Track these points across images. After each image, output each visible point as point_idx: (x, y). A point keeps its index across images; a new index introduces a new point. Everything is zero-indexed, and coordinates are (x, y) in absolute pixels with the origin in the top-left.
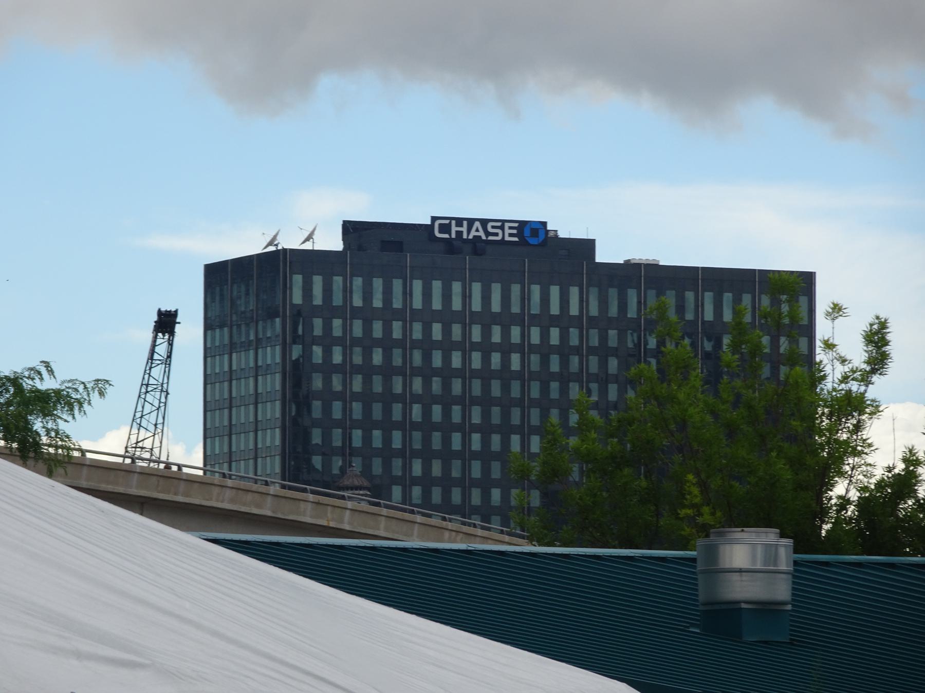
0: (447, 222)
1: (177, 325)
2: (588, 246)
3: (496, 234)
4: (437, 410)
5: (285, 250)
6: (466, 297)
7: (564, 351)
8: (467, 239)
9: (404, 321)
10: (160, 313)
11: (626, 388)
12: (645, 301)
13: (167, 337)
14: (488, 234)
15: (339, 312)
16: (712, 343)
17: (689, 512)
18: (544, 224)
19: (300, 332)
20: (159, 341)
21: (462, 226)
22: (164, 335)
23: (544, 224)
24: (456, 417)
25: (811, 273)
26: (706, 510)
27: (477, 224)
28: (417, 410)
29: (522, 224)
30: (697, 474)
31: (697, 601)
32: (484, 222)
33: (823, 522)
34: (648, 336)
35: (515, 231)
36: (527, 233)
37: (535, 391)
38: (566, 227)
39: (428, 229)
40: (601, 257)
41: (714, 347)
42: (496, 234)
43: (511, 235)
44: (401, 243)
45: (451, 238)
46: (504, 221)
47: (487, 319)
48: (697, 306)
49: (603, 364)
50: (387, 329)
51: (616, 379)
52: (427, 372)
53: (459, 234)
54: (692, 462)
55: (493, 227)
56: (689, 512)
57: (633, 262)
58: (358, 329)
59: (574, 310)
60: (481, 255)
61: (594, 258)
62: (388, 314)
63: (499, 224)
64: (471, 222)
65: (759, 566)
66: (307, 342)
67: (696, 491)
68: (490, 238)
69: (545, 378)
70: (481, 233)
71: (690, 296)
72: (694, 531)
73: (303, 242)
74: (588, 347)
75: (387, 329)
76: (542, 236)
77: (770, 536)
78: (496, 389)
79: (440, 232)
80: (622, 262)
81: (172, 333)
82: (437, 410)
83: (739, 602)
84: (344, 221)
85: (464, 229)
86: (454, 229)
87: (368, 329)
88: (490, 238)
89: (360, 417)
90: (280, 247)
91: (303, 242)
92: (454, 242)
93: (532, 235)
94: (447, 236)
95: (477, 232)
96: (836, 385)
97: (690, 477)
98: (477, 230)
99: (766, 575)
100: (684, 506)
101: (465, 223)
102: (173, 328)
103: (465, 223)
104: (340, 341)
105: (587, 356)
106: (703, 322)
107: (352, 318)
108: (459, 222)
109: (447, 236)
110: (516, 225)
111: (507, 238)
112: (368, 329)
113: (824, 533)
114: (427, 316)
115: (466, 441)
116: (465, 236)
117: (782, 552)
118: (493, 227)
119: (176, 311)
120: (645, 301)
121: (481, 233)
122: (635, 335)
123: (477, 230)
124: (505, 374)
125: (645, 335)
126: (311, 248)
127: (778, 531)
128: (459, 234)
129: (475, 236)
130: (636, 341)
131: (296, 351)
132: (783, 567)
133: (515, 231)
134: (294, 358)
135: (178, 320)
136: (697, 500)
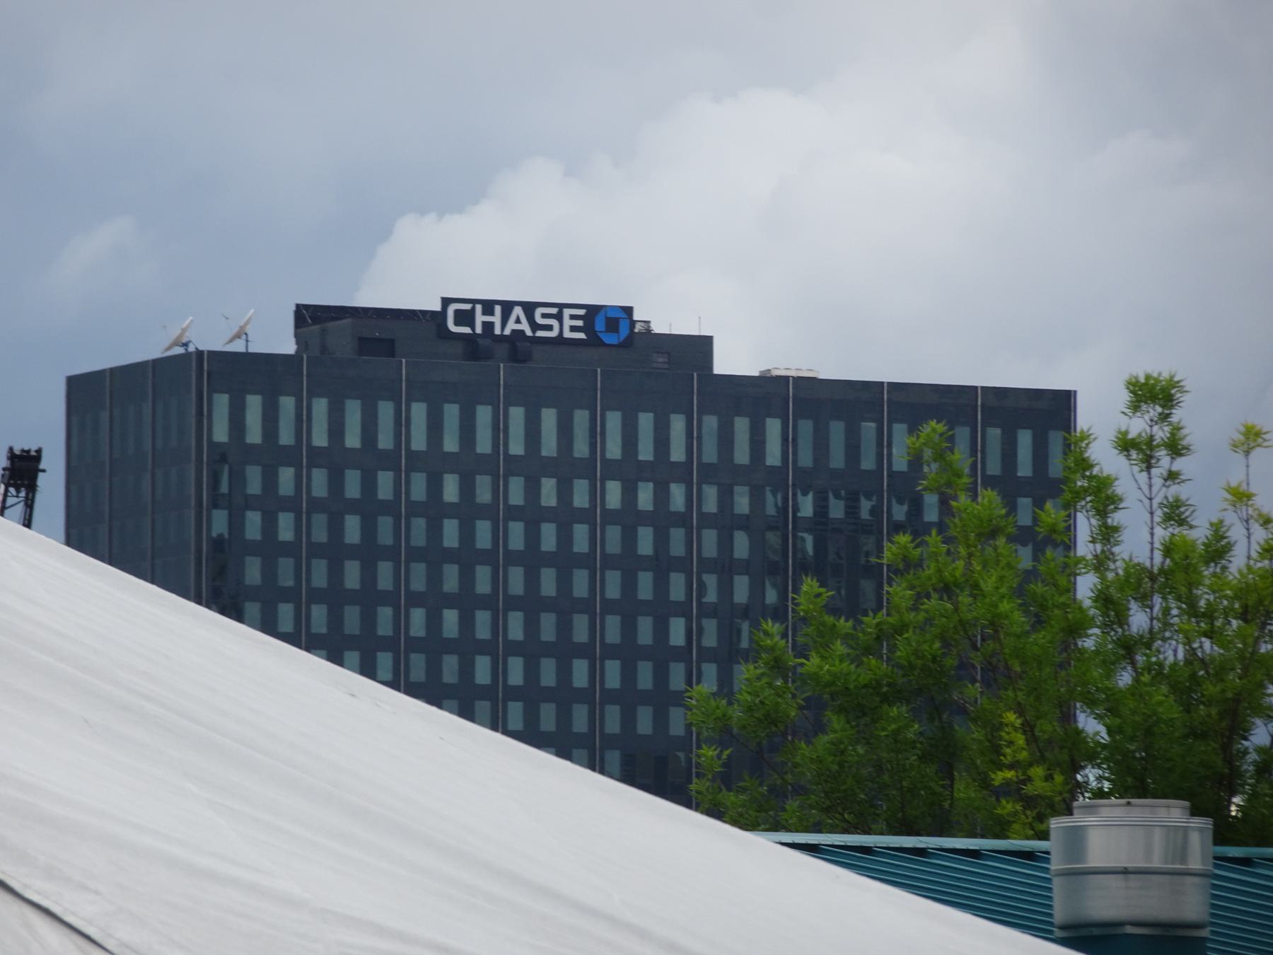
0: (468, 307)
1: (41, 475)
2: (701, 346)
3: (550, 328)
4: (451, 618)
5: (200, 354)
6: (499, 429)
7: (662, 519)
8: (502, 335)
9: (397, 470)
10: (12, 456)
11: (764, 583)
12: (794, 440)
13: (23, 494)
14: (535, 326)
15: (290, 456)
16: (905, 508)
17: (1010, 774)
18: (628, 311)
19: (224, 488)
20: (10, 501)
21: (492, 313)
22: (18, 491)
23: (628, 311)
24: (483, 630)
25: (1069, 392)
26: (1038, 772)
27: (518, 311)
28: (418, 617)
29: (592, 311)
30: (1020, 711)
31: (1051, 924)
32: (529, 308)
33: (1233, 794)
34: (800, 497)
35: (580, 323)
36: (600, 325)
37: (613, 588)
38: (665, 316)
39: (437, 318)
40: (726, 362)
41: (909, 514)
42: (550, 328)
43: (573, 329)
44: (392, 342)
45: (474, 334)
46: (561, 306)
47: (532, 467)
48: (880, 444)
49: (726, 543)
50: (369, 484)
51: (745, 567)
52: (435, 556)
53: (488, 326)
54: (1010, 693)
55: (544, 316)
56: (1010, 774)
57: (775, 373)
58: (319, 482)
59: (677, 453)
60: (523, 361)
61: (711, 368)
62: (371, 459)
63: (554, 311)
64: (507, 307)
65: (1156, 863)
66: (237, 507)
67: (1020, 740)
68: (540, 334)
69: (629, 563)
70: (525, 327)
71: (869, 428)
72: (1018, 807)
73: (231, 341)
74: (701, 515)
75: (369, 484)
76: (624, 331)
77: (1173, 813)
78: (548, 583)
79: (457, 323)
80: (756, 374)
81: (32, 488)
82: (451, 618)
83: (1121, 924)
84: (298, 306)
85: (496, 319)
86: (480, 318)
87: (336, 483)
88: (540, 334)
89: (324, 630)
90: (191, 349)
91: (231, 341)
92: (480, 341)
93: (609, 329)
94: (467, 330)
95: (518, 323)
96: (1252, 562)
97: (1011, 717)
98: (518, 321)
99: (1167, 877)
100: (1000, 766)
101: (498, 309)
102: (35, 478)
103: (498, 309)
104: (292, 504)
105: (699, 529)
106: (892, 474)
107: (311, 466)
108: (488, 306)
109: (467, 330)
110: (582, 312)
111: (568, 334)
112: (336, 483)
113: (1234, 810)
114: (434, 464)
115: (498, 670)
116: (497, 331)
117: (1195, 840)
118: (544, 316)
119: (39, 451)
120: (794, 440)
121: (525, 327)
122: (779, 496)
123: (518, 321)
124: (565, 561)
125: (794, 495)
126: (243, 350)
127: (1187, 804)
128: (488, 326)
129: (513, 331)
130: (780, 504)
131: (220, 523)
132: (1195, 864)
133: (580, 323)
134: (214, 535)
135: (42, 466)
136: (1024, 755)
